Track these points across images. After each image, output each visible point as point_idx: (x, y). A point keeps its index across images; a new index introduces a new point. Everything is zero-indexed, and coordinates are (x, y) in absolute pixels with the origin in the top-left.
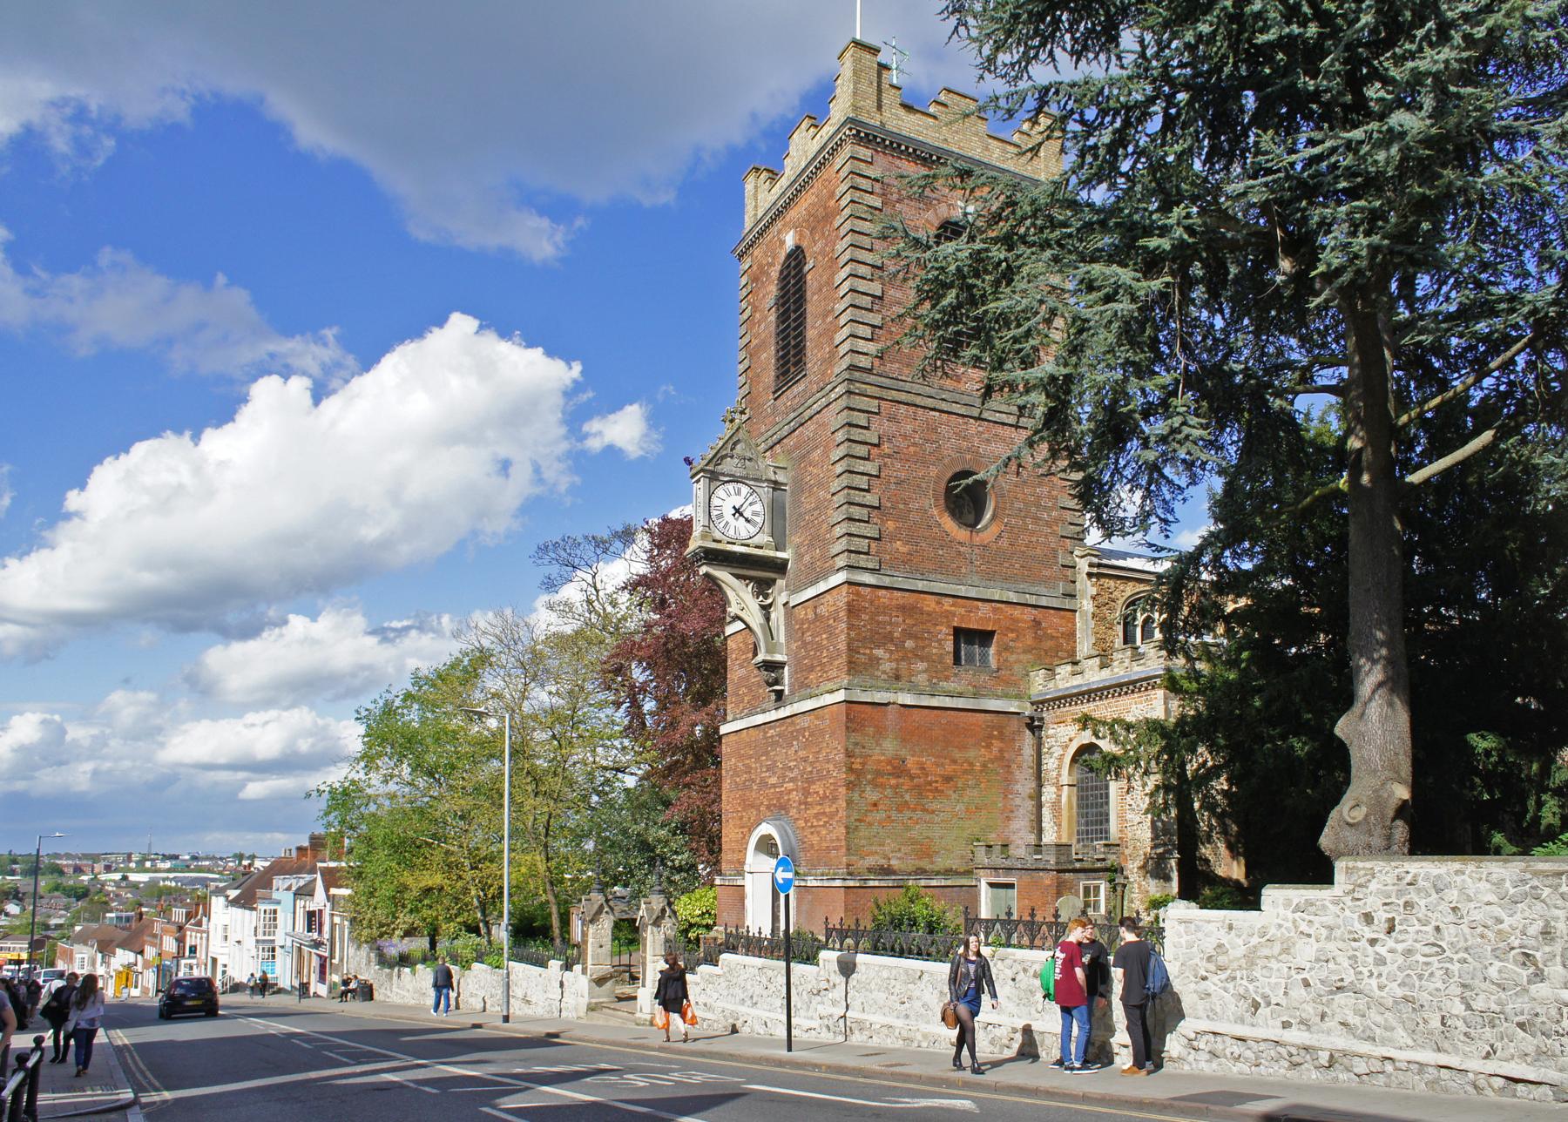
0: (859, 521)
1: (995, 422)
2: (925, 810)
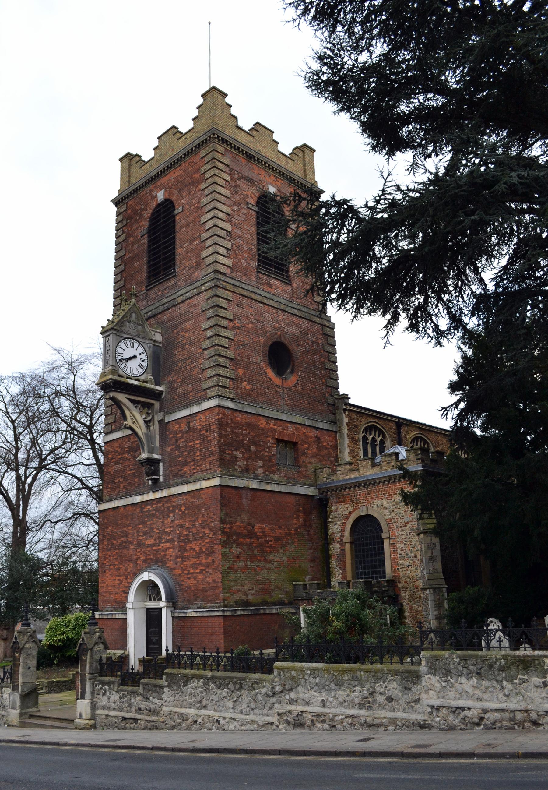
0: (224, 367)
1: (292, 314)
2: (266, 561)
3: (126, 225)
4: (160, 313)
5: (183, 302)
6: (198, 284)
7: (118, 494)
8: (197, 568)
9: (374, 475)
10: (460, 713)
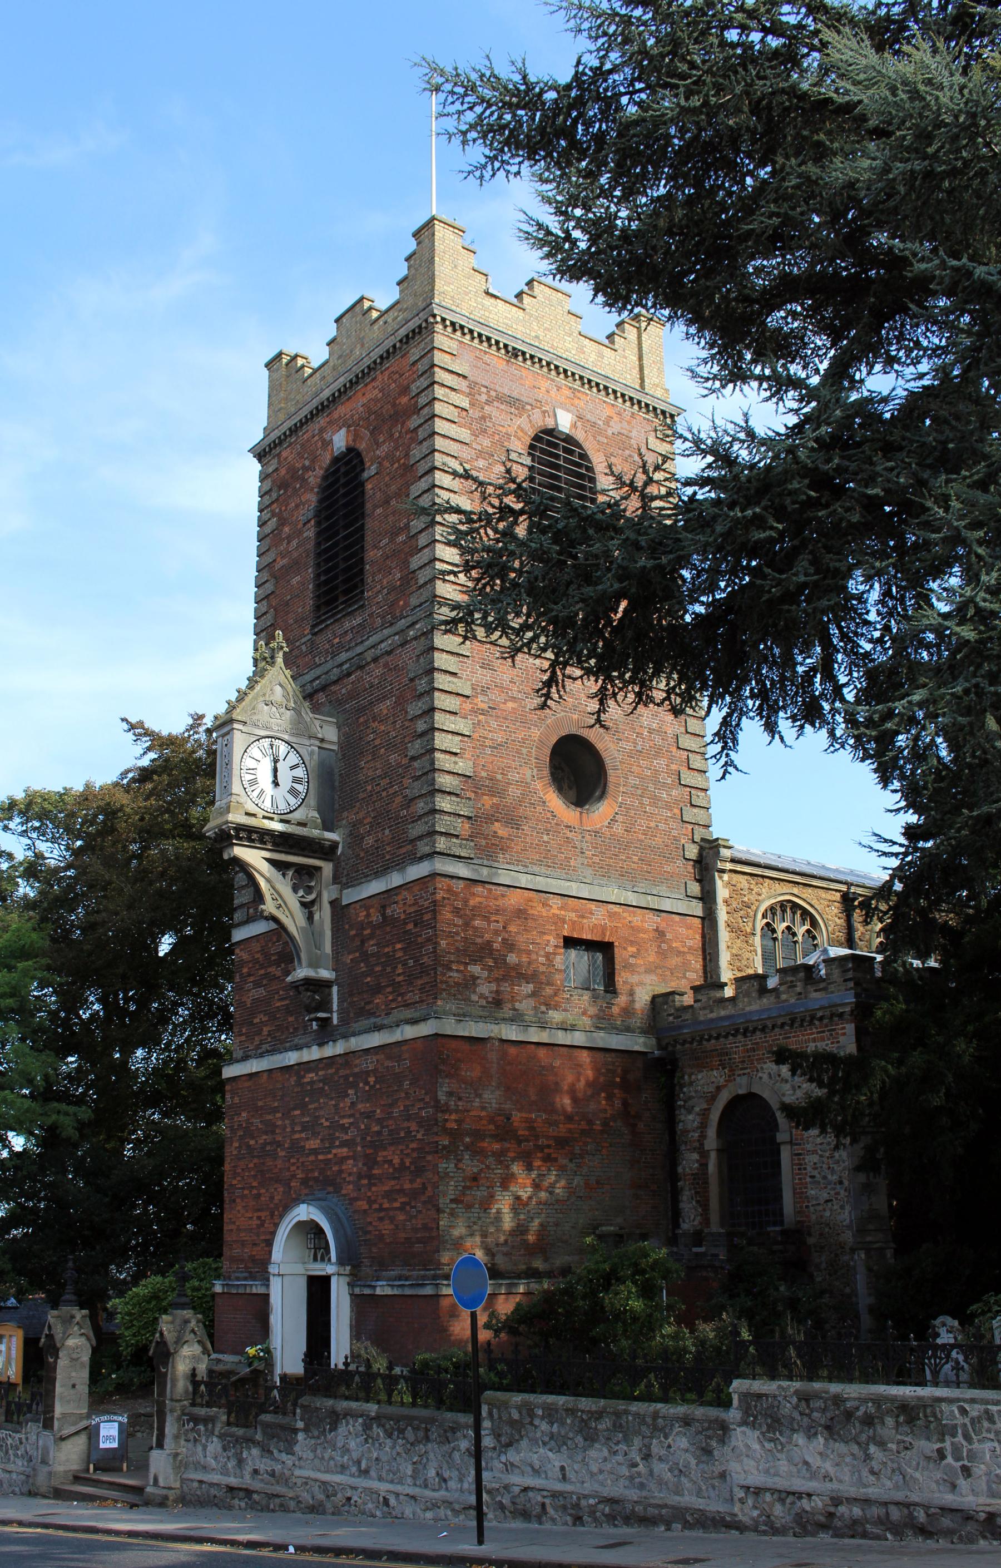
0: (450, 793)
3: (277, 500)
4: (335, 682)
5: (375, 660)
6: (402, 623)
7: (258, 1047)
8: (396, 1200)
9: (763, 1011)
10: (793, 1503)
